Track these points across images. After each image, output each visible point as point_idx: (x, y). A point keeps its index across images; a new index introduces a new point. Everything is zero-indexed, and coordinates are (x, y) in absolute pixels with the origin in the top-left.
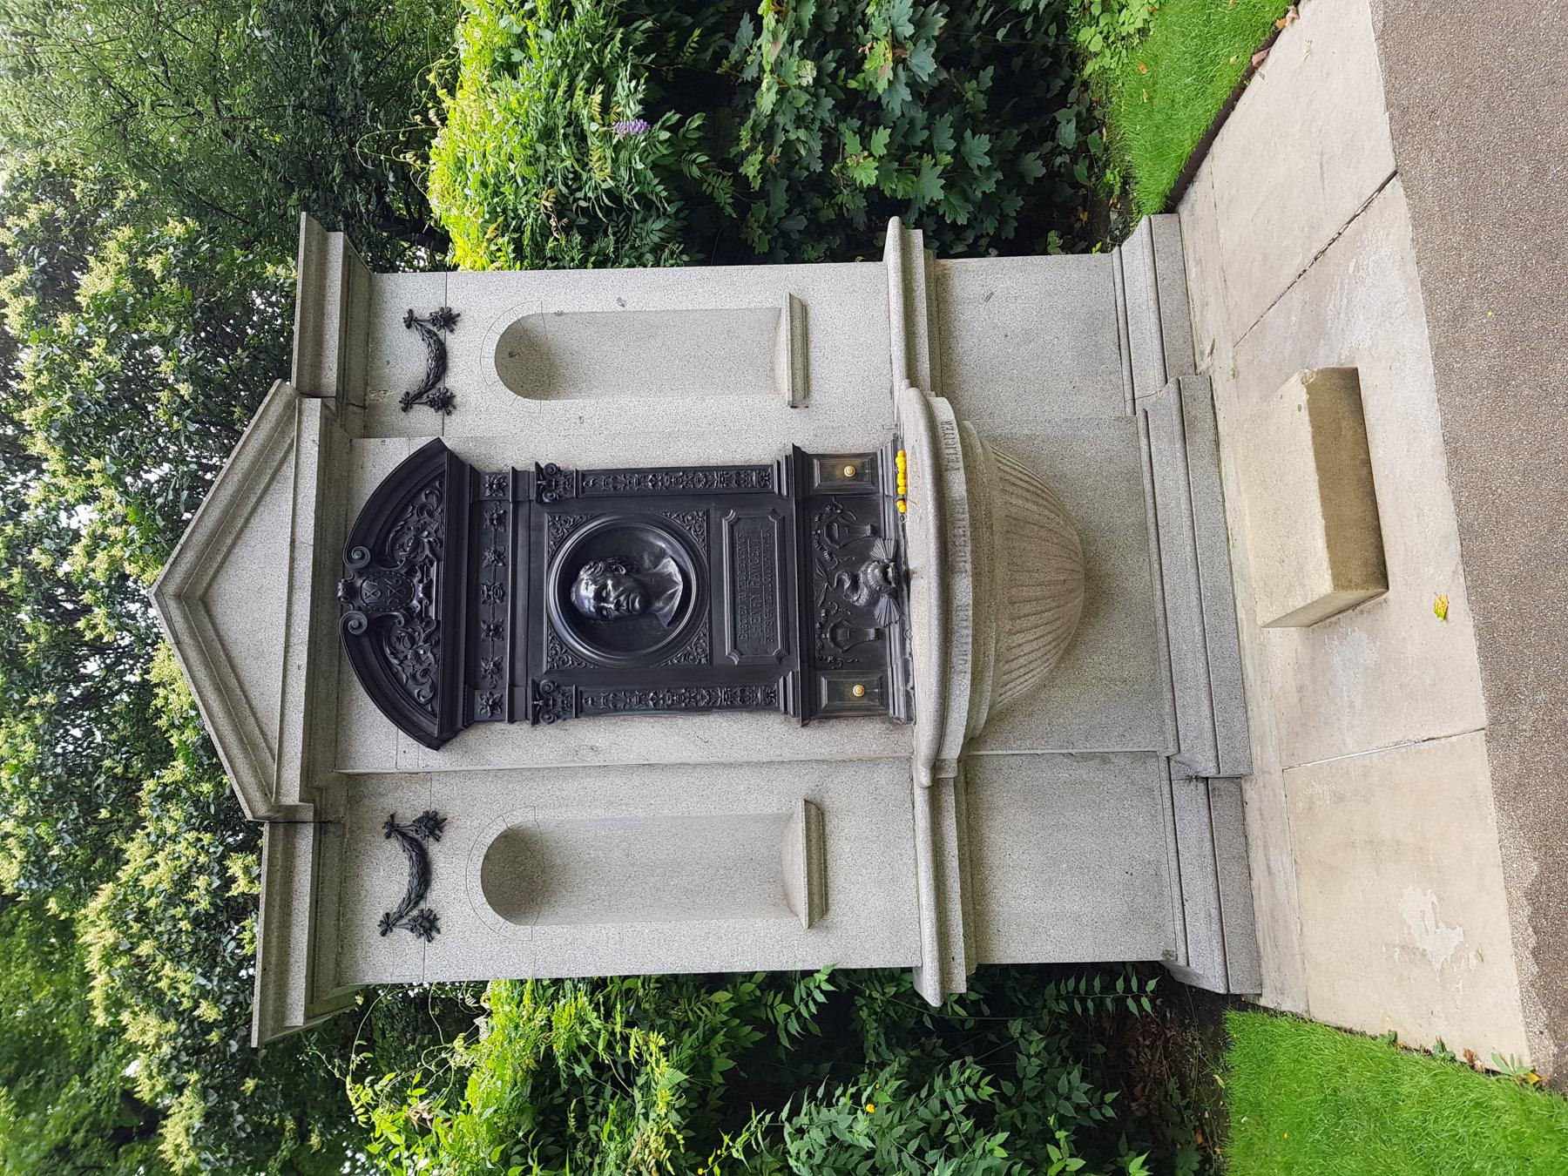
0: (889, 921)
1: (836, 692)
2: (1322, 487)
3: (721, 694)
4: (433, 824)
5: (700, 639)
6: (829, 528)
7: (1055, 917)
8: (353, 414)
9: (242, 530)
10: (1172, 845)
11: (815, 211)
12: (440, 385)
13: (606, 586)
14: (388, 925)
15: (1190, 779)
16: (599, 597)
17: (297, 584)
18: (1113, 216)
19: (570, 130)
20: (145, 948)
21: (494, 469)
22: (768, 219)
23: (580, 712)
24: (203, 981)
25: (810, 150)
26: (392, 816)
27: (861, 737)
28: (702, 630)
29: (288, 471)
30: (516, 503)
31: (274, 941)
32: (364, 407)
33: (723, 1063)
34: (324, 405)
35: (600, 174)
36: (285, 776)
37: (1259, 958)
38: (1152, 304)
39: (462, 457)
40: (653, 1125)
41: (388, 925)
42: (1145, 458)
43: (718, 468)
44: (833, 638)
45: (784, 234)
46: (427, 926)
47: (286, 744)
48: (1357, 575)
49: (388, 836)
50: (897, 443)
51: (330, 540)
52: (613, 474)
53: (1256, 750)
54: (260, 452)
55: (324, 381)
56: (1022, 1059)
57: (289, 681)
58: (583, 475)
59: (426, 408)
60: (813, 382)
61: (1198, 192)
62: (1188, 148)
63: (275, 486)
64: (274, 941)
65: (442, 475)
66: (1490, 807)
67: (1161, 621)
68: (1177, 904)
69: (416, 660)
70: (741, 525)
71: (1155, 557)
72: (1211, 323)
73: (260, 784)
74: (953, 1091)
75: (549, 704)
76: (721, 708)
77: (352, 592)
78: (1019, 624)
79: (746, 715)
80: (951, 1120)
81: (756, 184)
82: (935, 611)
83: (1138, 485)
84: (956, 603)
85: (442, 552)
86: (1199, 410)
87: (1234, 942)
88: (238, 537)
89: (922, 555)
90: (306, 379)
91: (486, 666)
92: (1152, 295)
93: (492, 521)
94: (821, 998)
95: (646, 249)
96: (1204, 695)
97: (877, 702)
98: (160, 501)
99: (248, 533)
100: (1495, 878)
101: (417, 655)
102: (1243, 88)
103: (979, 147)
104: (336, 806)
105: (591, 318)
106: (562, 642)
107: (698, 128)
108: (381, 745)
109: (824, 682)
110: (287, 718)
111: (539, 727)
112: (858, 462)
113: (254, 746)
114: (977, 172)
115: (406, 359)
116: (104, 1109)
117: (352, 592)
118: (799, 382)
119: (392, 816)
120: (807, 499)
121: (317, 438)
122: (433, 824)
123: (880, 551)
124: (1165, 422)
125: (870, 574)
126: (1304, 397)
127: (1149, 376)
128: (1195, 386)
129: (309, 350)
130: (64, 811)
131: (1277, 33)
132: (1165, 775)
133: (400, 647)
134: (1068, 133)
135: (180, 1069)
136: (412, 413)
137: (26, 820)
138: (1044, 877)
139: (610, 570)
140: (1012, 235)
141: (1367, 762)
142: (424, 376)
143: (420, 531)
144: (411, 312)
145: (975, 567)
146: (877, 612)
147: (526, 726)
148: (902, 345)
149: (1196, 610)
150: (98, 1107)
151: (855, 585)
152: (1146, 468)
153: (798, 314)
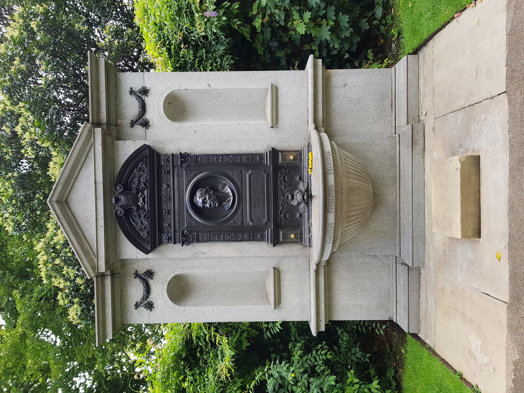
0: (300, 306)
1: (285, 236)
2: (462, 201)
3: (246, 236)
4: (150, 274)
5: (238, 216)
6: (284, 177)
7: (355, 306)
8: (113, 132)
9: (77, 176)
10: (395, 284)
11: (281, 37)
12: (144, 117)
13: (205, 198)
14: (137, 306)
15: (403, 264)
16: (204, 202)
17: (98, 197)
18: (393, 46)
19: (188, 10)
20: (57, 261)
21: (165, 153)
22: (263, 41)
23: (198, 241)
24: (77, 273)
25: (280, 17)
26: (136, 271)
27: (294, 250)
28: (239, 213)
29: (91, 154)
30: (173, 167)
31: (101, 314)
32: (117, 126)
33: (246, 344)
34: (102, 130)
35: (200, 30)
36: (99, 263)
37: (420, 322)
38: (405, 91)
39: (154, 148)
40: (224, 364)
41: (137, 306)
42: (398, 153)
43: (245, 155)
44: (285, 217)
45: (269, 47)
46: (150, 306)
47: (99, 253)
48: (470, 233)
49: (135, 278)
50: (309, 145)
51: (108, 179)
52: (207, 156)
53: (426, 260)
54: (81, 149)
55: (102, 118)
56: (340, 341)
57: (98, 231)
58: (197, 156)
59: (139, 126)
60: (279, 120)
61: (426, 50)
62: (425, 36)
63: (87, 160)
64: (101, 314)
65: (147, 157)
66: (505, 329)
67: (398, 212)
68: (395, 303)
69: (142, 224)
70: (253, 176)
71: (398, 189)
72: (426, 104)
73: (91, 267)
74: (319, 356)
75: (186, 240)
76: (246, 240)
77: (117, 200)
78: (349, 224)
79: (254, 242)
80: (318, 365)
81: (259, 30)
82: (321, 226)
83: (394, 161)
84: (328, 222)
85: (148, 185)
86: (418, 137)
87: (412, 317)
88: (76, 179)
89: (317, 190)
90: (95, 118)
91: (166, 225)
92: (406, 88)
93: (165, 173)
94: (278, 330)
95: (218, 57)
96: (411, 240)
97: (299, 240)
98: (46, 119)
99: (80, 178)
100: (503, 352)
101: (141, 222)
102: (449, 22)
103: (344, 19)
104: (117, 269)
105: (198, 91)
106: (191, 217)
107: (237, 9)
108: (130, 251)
109: (281, 233)
110: (99, 244)
111: (184, 245)
112: (295, 154)
113: (88, 253)
114: (343, 28)
115: (130, 107)
116: (49, 293)
117: (117, 200)
118: (274, 119)
119: (136, 271)
120: (276, 167)
121: (101, 143)
122: (150, 274)
123: (302, 187)
124: (406, 140)
125: (298, 197)
126: (459, 166)
127: (402, 119)
128: (418, 127)
129: (95, 106)
130: (25, 211)
131: (465, 9)
132: (394, 261)
133: (136, 219)
134: (379, 12)
135: (72, 297)
136: (134, 128)
137: (11, 214)
138: (352, 293)
139: (207, 192)
140: (354, 50)
141: (465, 288)
142: (137, 114)
143: (140, 177)
144: (131, 88)
145: (335, 209)
146: (300, 208)
147: (180, 245)
148: (312, 107)
149: (411, 210)
150: (47, 293)
151: (293, 198)
152: (398, 156)
153: (274, 92)
